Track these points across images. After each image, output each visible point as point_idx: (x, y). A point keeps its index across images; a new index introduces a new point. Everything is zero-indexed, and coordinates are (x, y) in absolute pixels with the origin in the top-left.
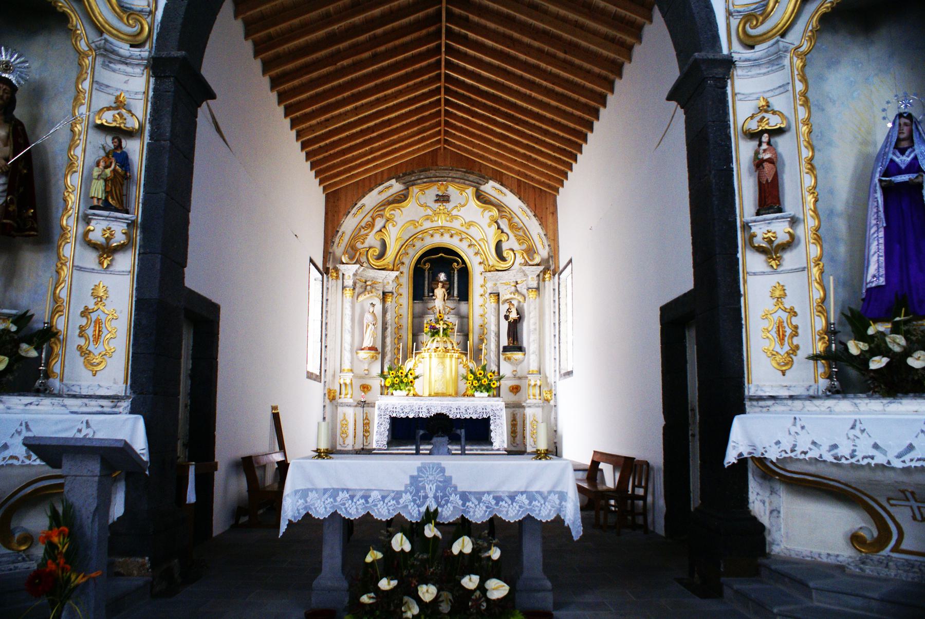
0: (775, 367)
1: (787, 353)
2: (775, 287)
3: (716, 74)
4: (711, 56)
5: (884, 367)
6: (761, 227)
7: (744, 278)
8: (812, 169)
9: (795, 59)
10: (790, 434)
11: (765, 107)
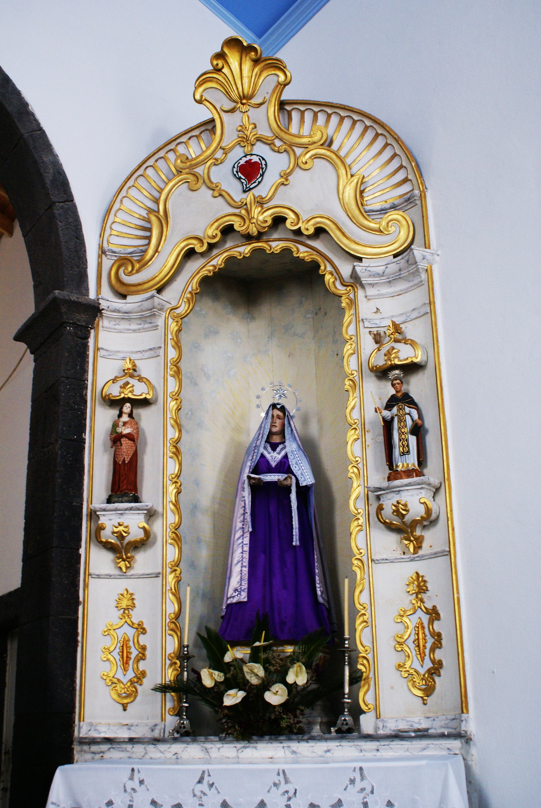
0: (114, 700)
1: (131, 681)
2: (122, 595)
3: (78, 320)
4: (74, 298)
5: (240, 702)
6: (111, 518)
7: (84, 581)
8: (177, 453)
9: (170, 320)
10: (125, 791)
11: (131, 371)
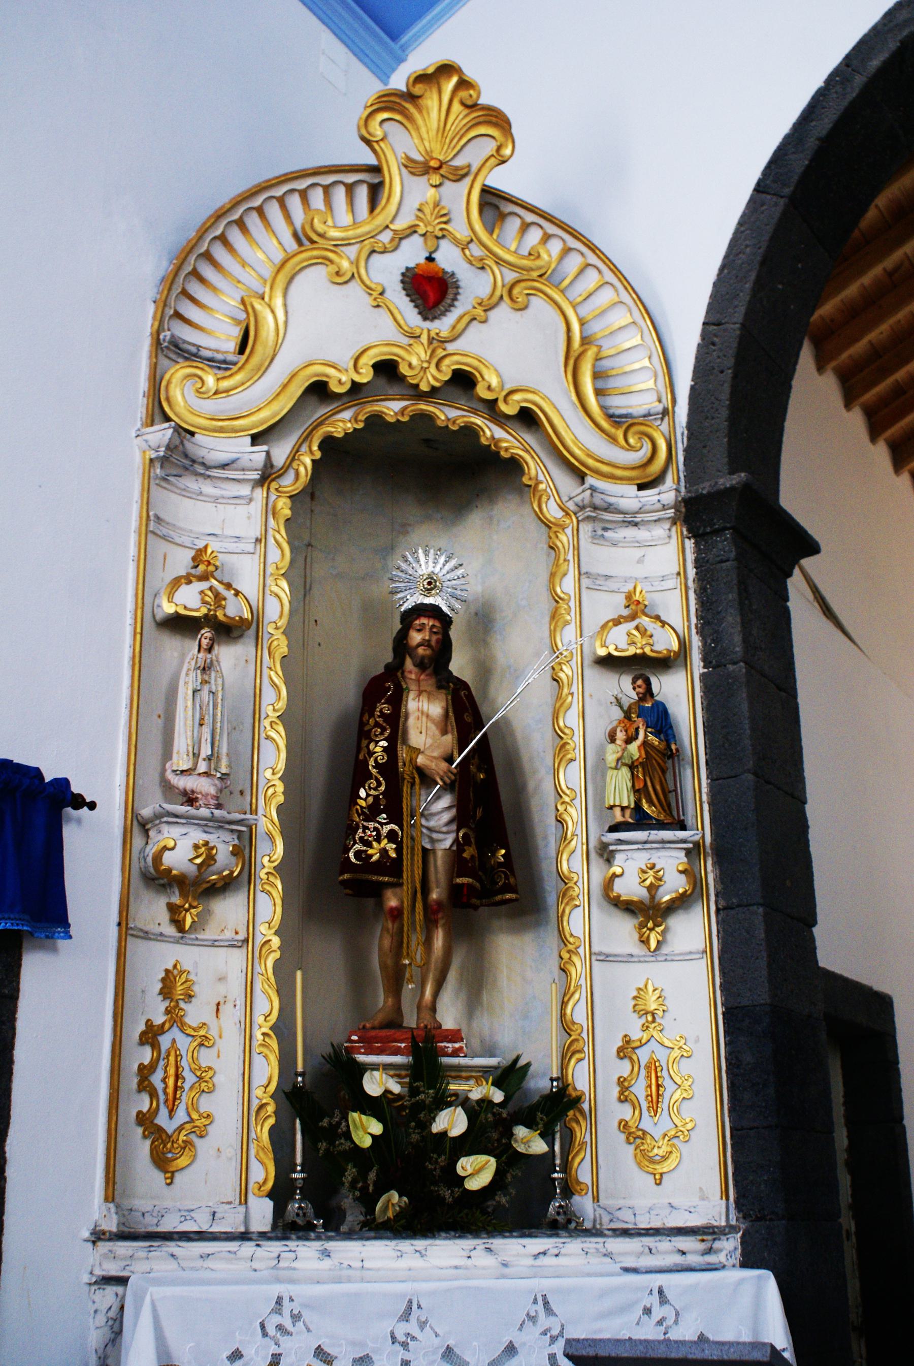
10: (265, 1334)
